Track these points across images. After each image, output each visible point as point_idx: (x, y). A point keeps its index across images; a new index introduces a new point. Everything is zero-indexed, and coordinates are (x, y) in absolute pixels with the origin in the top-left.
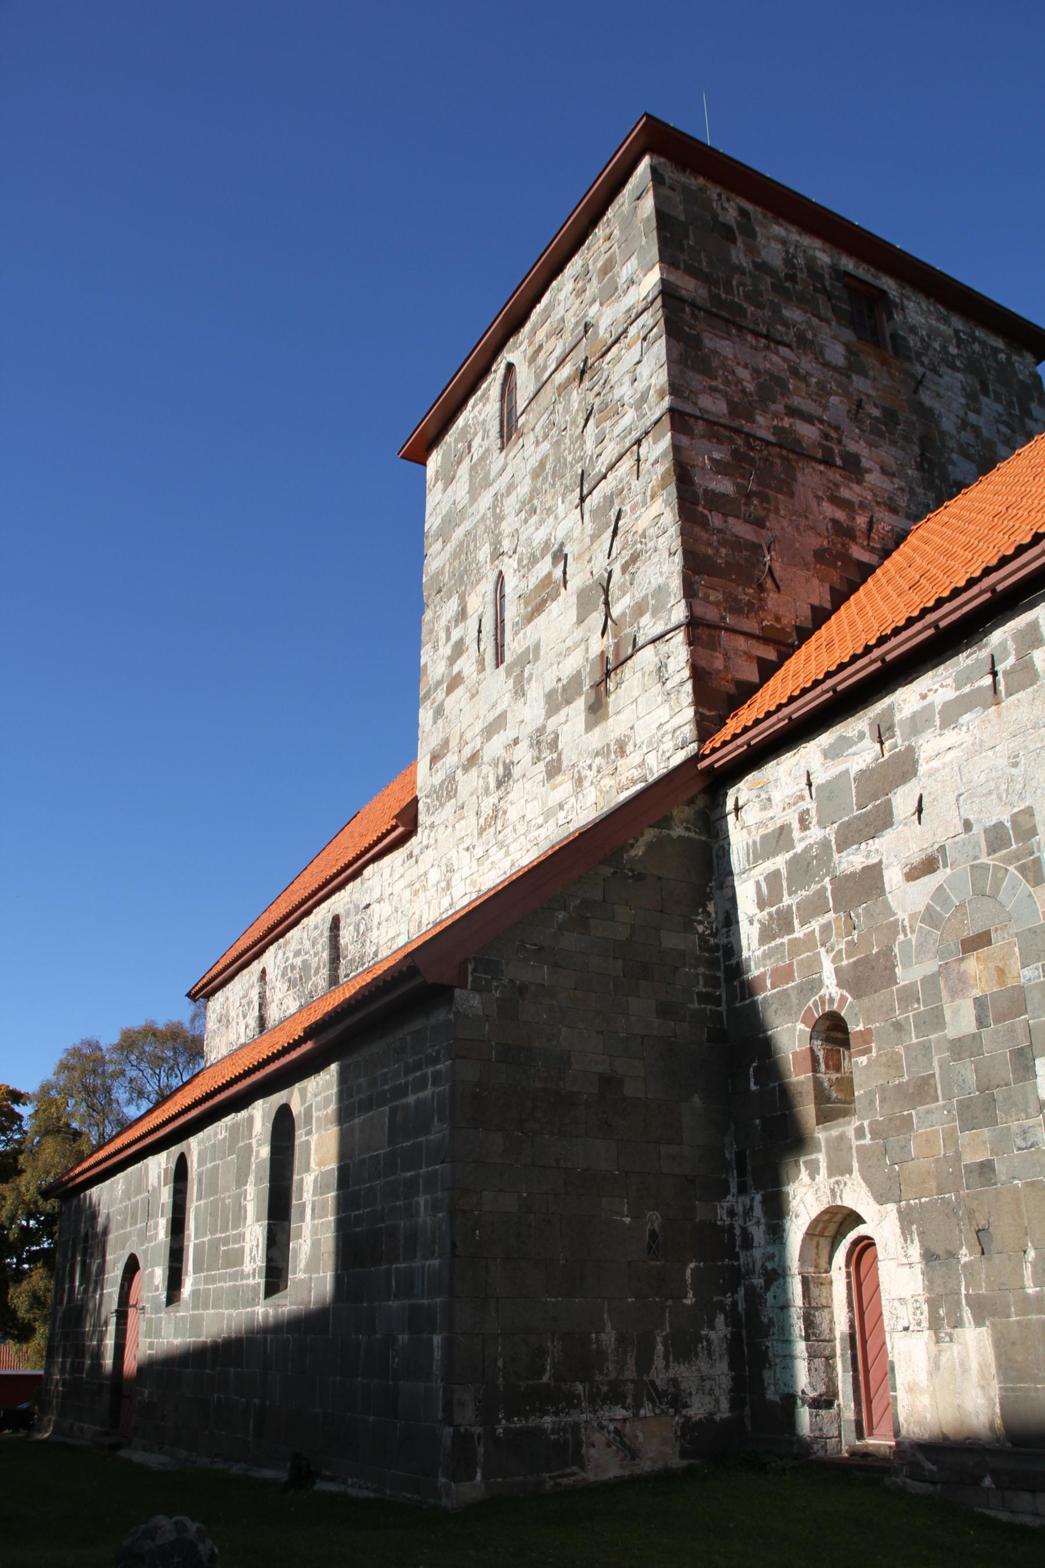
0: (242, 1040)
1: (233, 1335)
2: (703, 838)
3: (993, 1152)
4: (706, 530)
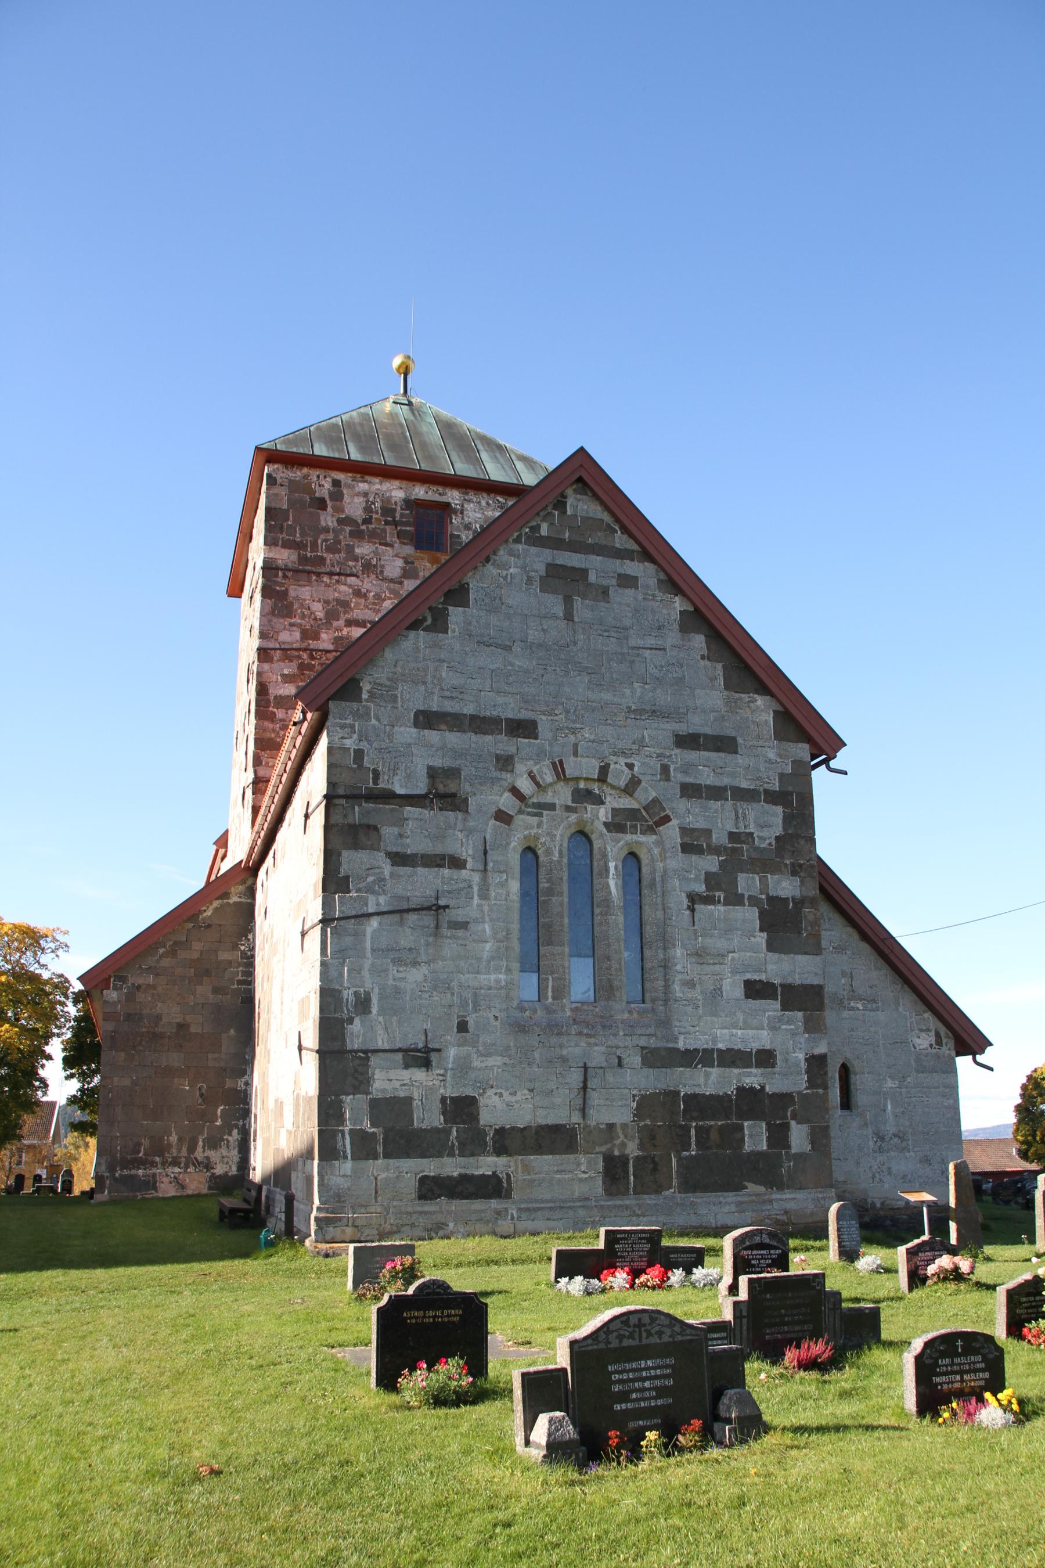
2: (249, 901)
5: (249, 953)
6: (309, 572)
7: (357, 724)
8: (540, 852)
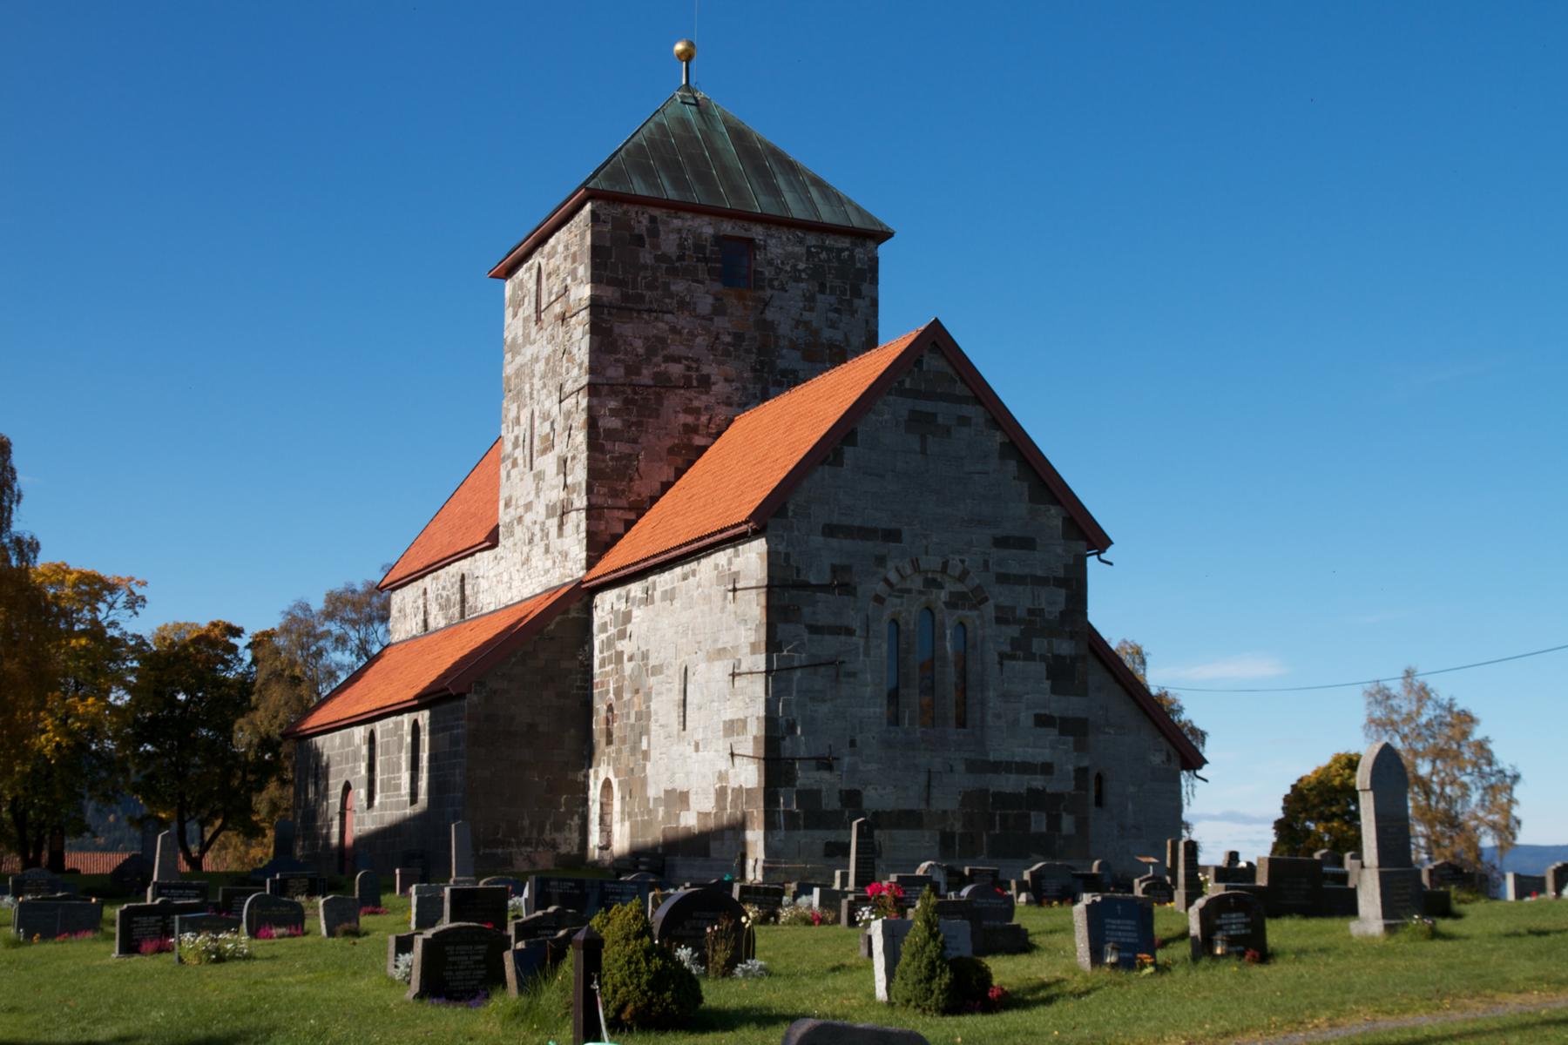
0: (414, 632)
5: (586, 663)
6: (631, 310)
7: (785, 534)
8: (900, 623)
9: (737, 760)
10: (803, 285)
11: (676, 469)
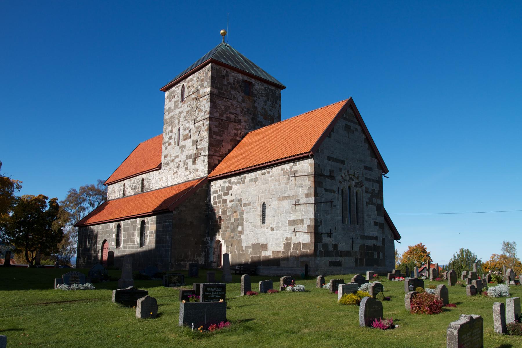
0: (119, 197)
1: (133, 253)
2: (207, 188)
3: (234, 235)
4: (213, 139)
6: (221, 97)
9: (297, 234)
10: (264, 98)
11: (232, 146)
